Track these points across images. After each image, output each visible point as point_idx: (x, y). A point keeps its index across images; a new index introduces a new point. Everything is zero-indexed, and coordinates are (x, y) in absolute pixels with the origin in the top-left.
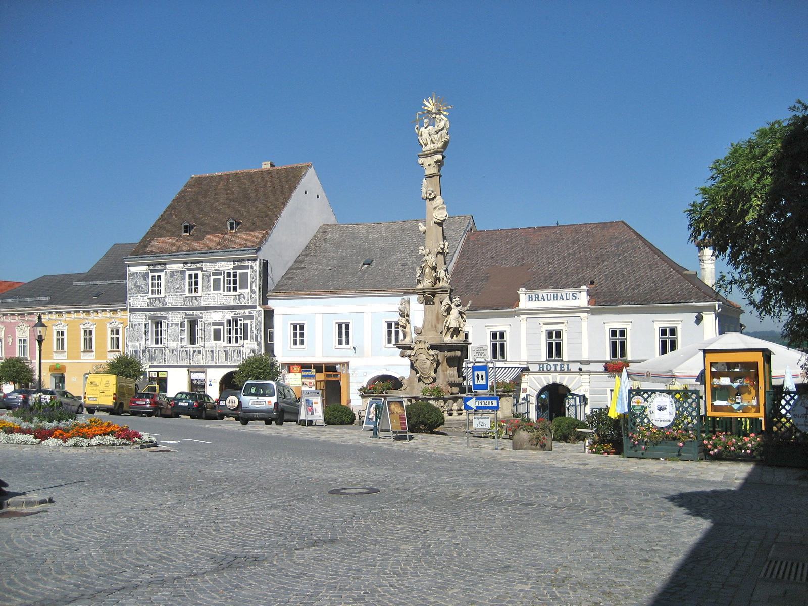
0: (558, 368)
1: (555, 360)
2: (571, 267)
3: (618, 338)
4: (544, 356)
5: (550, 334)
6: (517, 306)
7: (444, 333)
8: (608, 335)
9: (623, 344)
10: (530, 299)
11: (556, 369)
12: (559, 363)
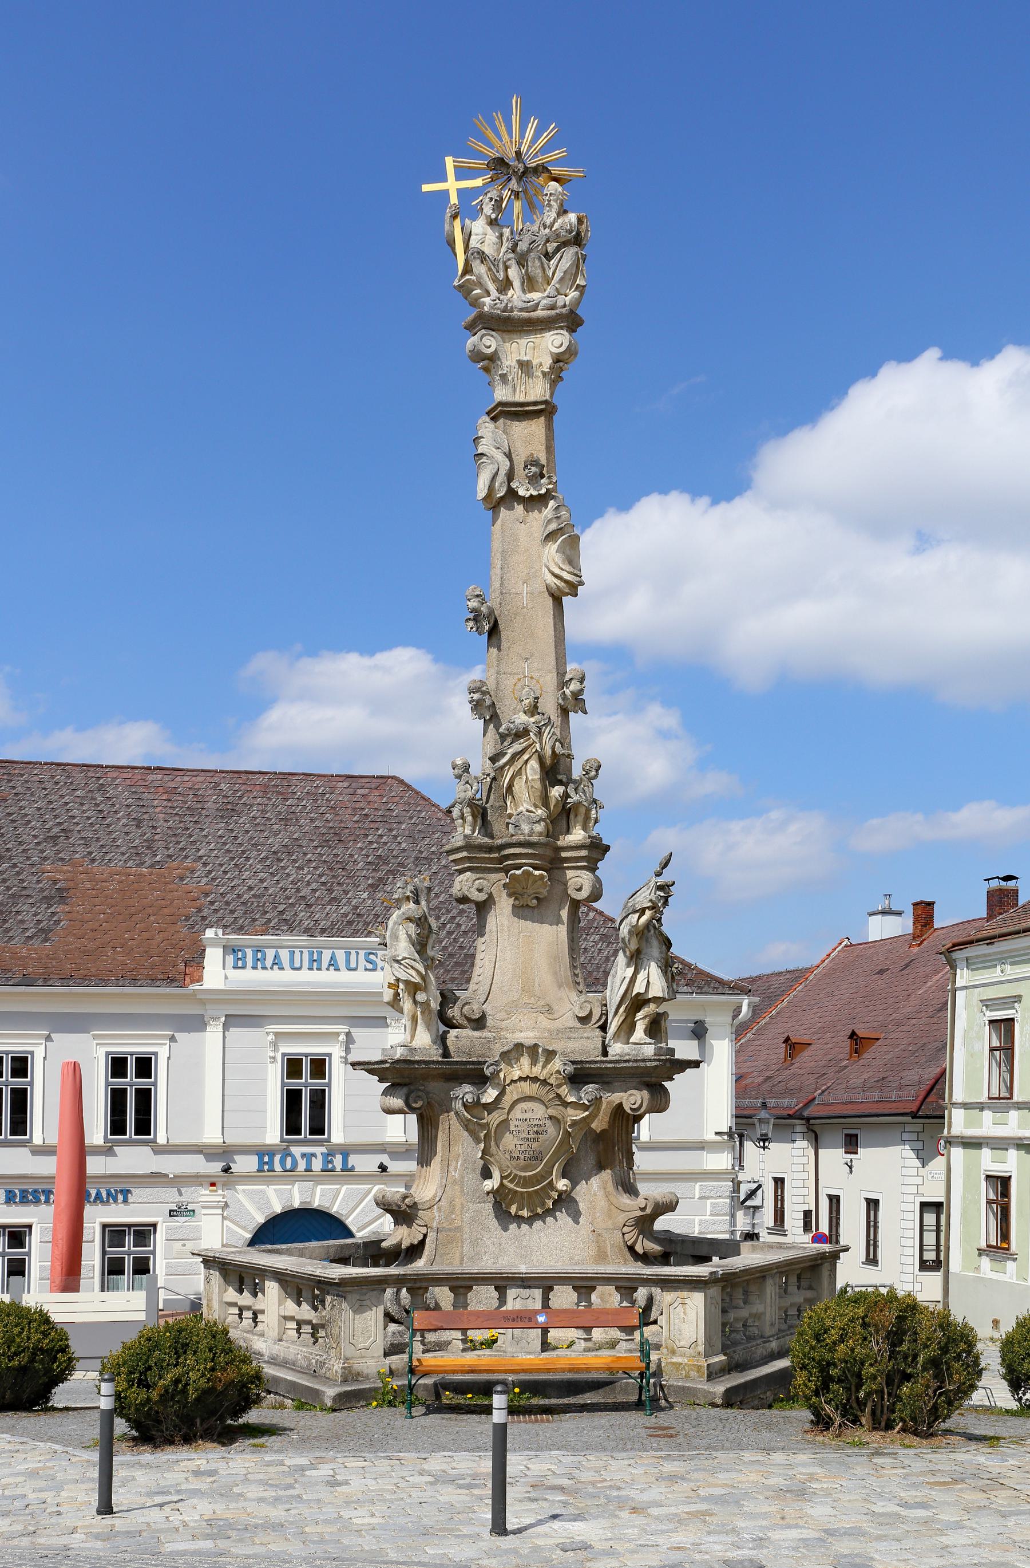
0: (317, 1165)
1: (305, 1143)
3: (131, 1082)
4: (273, 1133)
5: (293, 1067)
9: (144, 1098)
11: (308, 1169)
12: (319, 1150)
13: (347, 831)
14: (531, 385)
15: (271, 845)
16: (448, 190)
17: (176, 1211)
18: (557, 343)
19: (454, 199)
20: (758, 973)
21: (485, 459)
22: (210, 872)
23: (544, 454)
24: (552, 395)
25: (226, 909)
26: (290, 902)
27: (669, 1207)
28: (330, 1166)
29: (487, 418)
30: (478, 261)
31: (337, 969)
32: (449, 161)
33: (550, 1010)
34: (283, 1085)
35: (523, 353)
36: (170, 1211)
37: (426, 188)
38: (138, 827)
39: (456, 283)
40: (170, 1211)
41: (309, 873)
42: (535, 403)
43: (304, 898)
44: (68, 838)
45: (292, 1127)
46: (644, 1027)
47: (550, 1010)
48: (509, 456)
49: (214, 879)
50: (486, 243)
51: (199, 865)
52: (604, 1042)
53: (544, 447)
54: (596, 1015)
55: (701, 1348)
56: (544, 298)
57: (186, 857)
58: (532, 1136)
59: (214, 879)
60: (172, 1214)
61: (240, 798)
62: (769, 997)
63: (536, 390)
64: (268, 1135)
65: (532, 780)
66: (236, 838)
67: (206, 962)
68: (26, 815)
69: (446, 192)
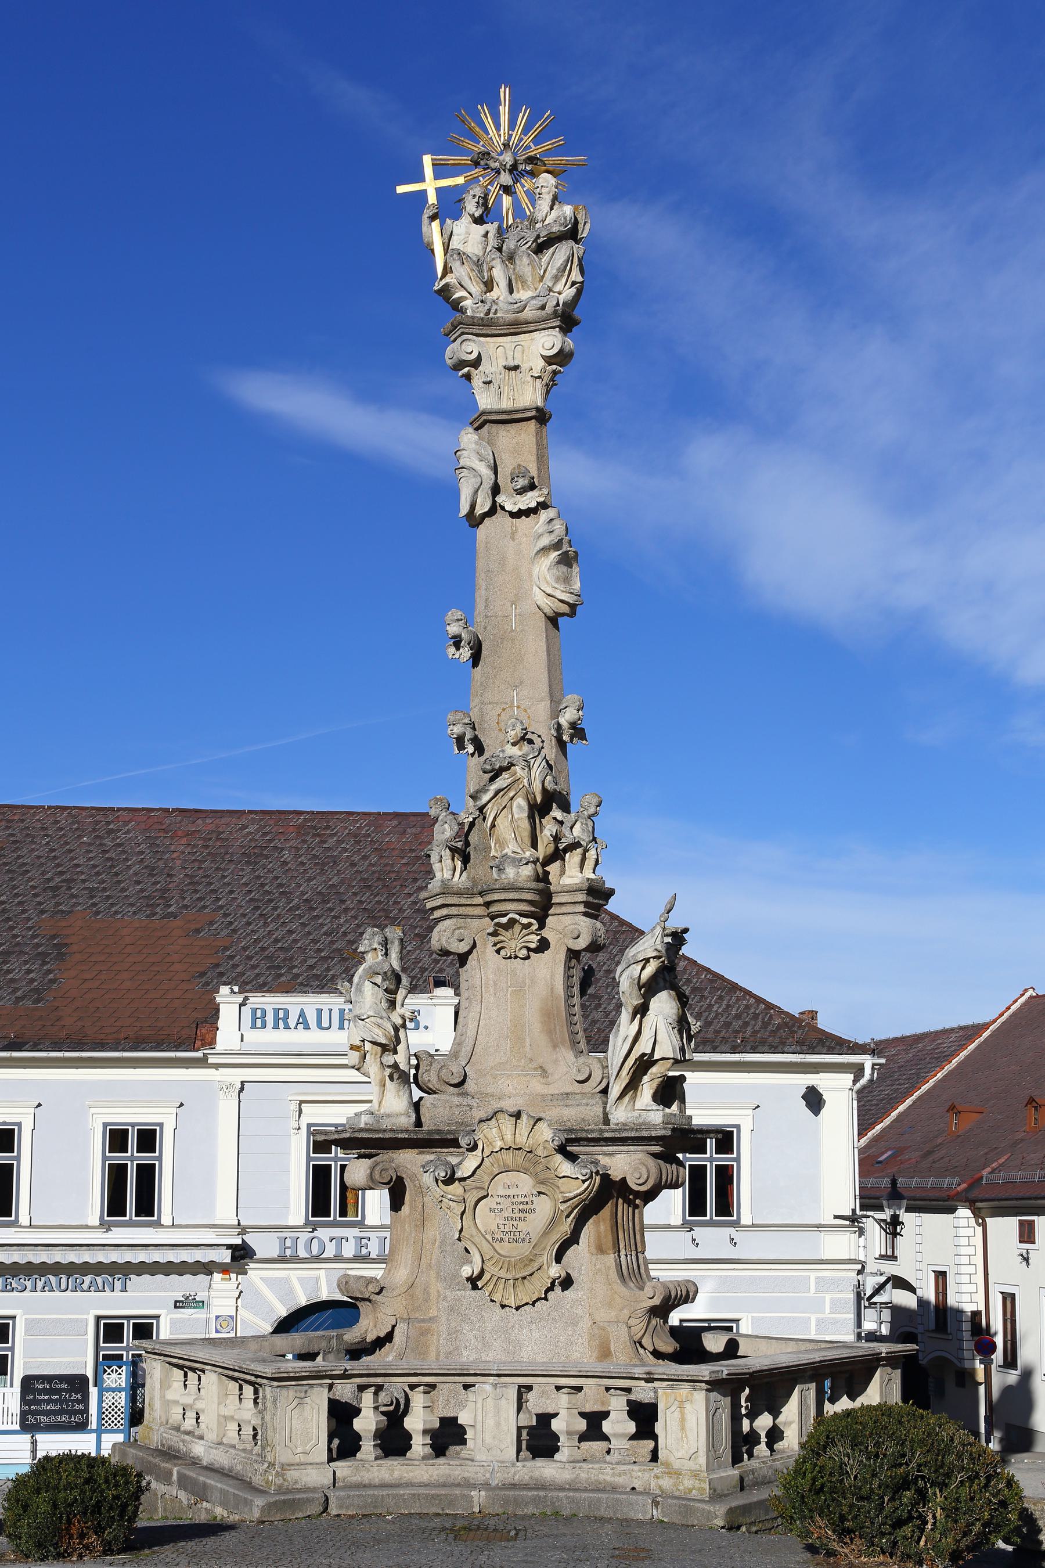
1: (334, 1225)
2: (345, 934)
6: (212, 1043)
7: (615, 1091)
8: (97, 1142)
9: (147, 1176)
10: (258, 1020)
13: (393, 876)
14: (520, 391)
15: (303, 893)
16: (426, 190)
17: (182, 1302)
18: (549, 345)
19: (432, 198)
20: (925, 1030)
21: (465, 472)
22: (231, 923)
23: (535, 464)
24: (545, 400)
25: (247, 964)
26: (322, 954)
27: (687, 1296)
28: (364, 1251)
29: (471, 430)
30: (458, 263)
31: (307, 1027)
32: (427, 160)
33: (544, 1073)
34: (309, 1159)
35: (510, 358)
36: (176, 1302)
37: (401, 189)
38: (151, 875)
39: (435, 288)
40: (176, 1302)
41: (346, 922)
42: (524, 410)
43: (339, 950)
44: (69, 888)
45: (319, 1205)
46: (652, 1091)
47: (544, 1073)
48: (495, 470)
49: (234, 931)
50: (469, 243)
51: (219, 917)
52: (605, 1108)
53: (535, 457)
54: (597, 1076)
55: (702, 1460)
56: (533, 298)
57: (205, 907)
58: (517, 1215)
59: (234, 931)
60: (177, 1305)
61: (270, 841)
62: (937, 1058)
63: (530, 396)
64: (290, 1218)
65: (519, 819)
66: (263, 885)
67: (221, 1023)
68: (24, 864)
69: (424, 193)
